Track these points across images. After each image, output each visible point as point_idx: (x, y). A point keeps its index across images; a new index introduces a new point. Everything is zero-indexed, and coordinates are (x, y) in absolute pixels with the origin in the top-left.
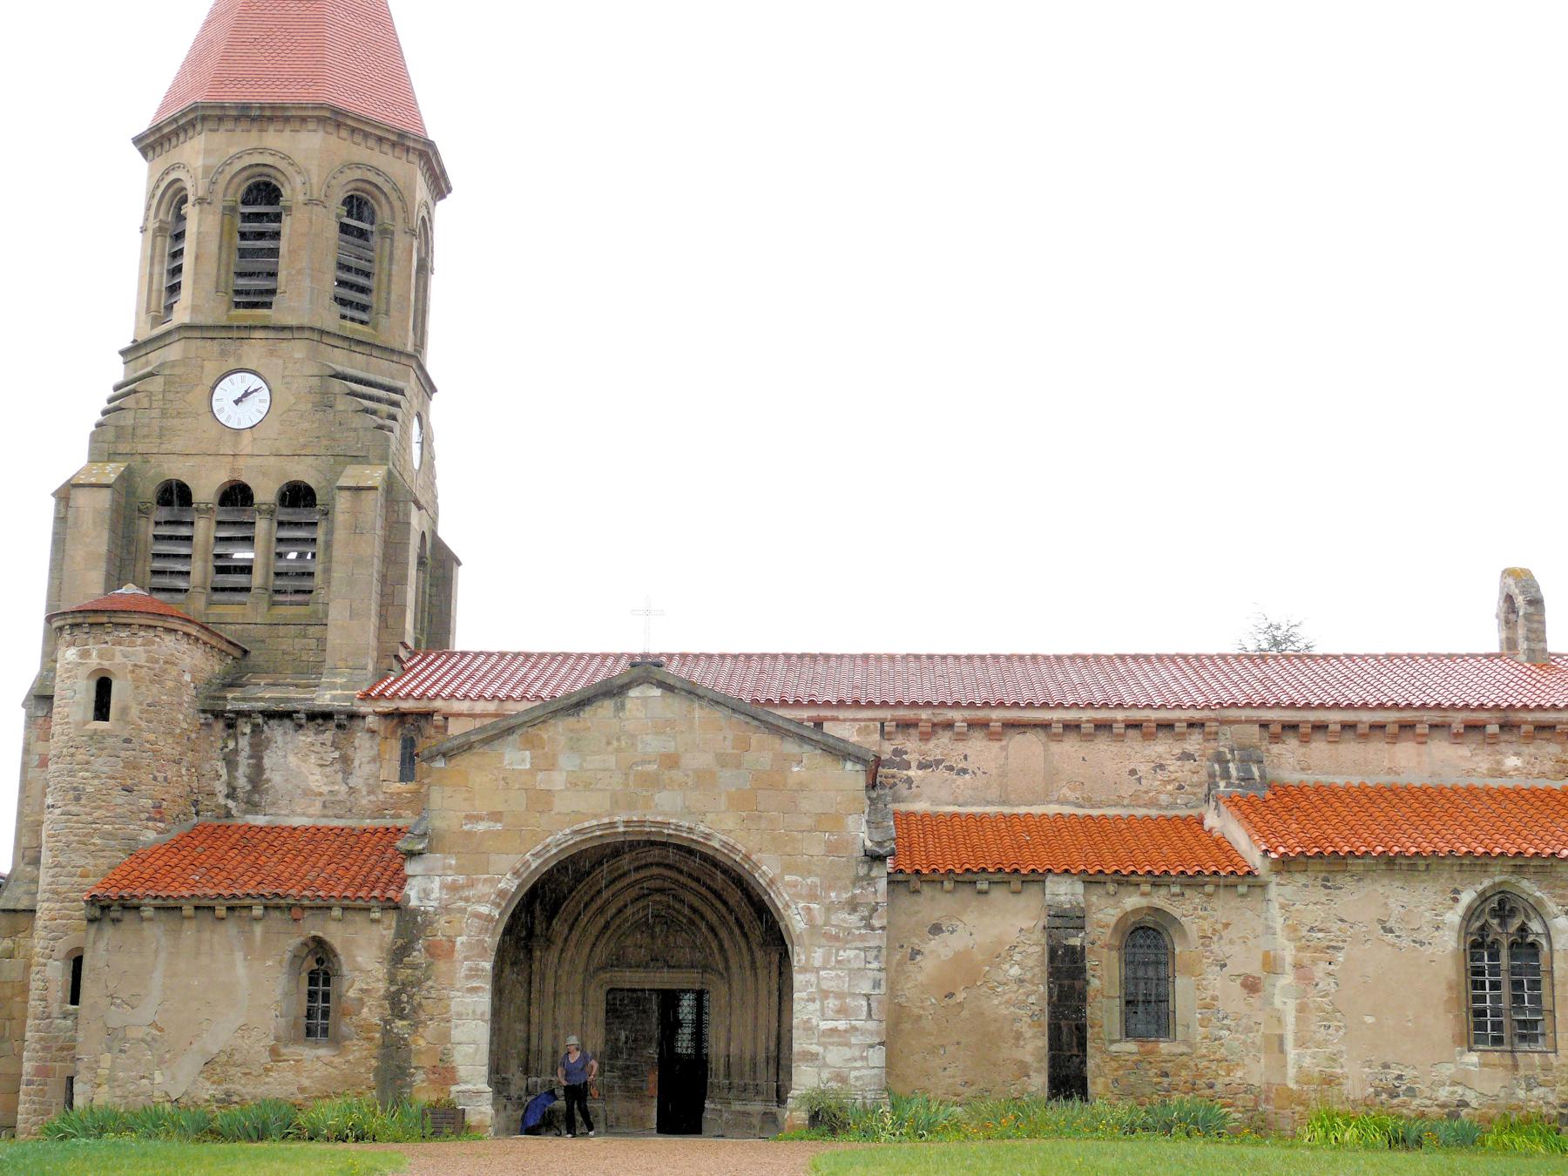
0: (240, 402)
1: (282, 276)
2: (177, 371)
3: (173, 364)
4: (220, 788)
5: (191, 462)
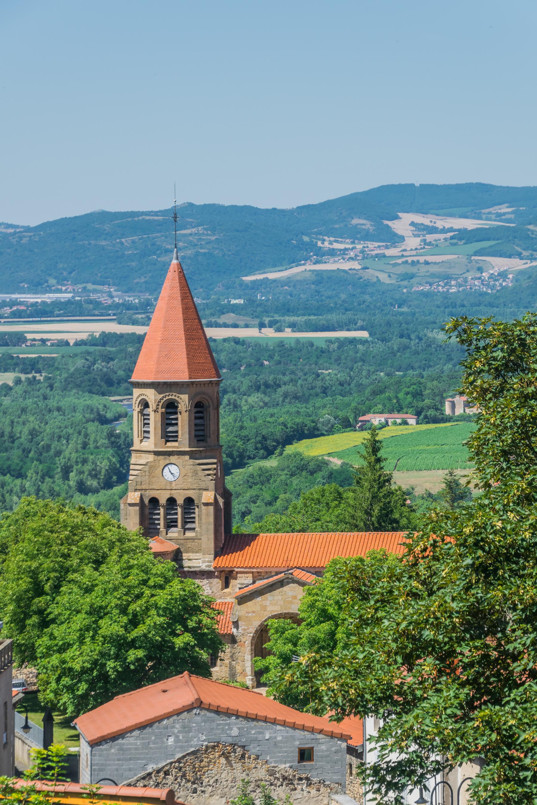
1: (180, 432)
2: (153, 464)
3: (151, 462)
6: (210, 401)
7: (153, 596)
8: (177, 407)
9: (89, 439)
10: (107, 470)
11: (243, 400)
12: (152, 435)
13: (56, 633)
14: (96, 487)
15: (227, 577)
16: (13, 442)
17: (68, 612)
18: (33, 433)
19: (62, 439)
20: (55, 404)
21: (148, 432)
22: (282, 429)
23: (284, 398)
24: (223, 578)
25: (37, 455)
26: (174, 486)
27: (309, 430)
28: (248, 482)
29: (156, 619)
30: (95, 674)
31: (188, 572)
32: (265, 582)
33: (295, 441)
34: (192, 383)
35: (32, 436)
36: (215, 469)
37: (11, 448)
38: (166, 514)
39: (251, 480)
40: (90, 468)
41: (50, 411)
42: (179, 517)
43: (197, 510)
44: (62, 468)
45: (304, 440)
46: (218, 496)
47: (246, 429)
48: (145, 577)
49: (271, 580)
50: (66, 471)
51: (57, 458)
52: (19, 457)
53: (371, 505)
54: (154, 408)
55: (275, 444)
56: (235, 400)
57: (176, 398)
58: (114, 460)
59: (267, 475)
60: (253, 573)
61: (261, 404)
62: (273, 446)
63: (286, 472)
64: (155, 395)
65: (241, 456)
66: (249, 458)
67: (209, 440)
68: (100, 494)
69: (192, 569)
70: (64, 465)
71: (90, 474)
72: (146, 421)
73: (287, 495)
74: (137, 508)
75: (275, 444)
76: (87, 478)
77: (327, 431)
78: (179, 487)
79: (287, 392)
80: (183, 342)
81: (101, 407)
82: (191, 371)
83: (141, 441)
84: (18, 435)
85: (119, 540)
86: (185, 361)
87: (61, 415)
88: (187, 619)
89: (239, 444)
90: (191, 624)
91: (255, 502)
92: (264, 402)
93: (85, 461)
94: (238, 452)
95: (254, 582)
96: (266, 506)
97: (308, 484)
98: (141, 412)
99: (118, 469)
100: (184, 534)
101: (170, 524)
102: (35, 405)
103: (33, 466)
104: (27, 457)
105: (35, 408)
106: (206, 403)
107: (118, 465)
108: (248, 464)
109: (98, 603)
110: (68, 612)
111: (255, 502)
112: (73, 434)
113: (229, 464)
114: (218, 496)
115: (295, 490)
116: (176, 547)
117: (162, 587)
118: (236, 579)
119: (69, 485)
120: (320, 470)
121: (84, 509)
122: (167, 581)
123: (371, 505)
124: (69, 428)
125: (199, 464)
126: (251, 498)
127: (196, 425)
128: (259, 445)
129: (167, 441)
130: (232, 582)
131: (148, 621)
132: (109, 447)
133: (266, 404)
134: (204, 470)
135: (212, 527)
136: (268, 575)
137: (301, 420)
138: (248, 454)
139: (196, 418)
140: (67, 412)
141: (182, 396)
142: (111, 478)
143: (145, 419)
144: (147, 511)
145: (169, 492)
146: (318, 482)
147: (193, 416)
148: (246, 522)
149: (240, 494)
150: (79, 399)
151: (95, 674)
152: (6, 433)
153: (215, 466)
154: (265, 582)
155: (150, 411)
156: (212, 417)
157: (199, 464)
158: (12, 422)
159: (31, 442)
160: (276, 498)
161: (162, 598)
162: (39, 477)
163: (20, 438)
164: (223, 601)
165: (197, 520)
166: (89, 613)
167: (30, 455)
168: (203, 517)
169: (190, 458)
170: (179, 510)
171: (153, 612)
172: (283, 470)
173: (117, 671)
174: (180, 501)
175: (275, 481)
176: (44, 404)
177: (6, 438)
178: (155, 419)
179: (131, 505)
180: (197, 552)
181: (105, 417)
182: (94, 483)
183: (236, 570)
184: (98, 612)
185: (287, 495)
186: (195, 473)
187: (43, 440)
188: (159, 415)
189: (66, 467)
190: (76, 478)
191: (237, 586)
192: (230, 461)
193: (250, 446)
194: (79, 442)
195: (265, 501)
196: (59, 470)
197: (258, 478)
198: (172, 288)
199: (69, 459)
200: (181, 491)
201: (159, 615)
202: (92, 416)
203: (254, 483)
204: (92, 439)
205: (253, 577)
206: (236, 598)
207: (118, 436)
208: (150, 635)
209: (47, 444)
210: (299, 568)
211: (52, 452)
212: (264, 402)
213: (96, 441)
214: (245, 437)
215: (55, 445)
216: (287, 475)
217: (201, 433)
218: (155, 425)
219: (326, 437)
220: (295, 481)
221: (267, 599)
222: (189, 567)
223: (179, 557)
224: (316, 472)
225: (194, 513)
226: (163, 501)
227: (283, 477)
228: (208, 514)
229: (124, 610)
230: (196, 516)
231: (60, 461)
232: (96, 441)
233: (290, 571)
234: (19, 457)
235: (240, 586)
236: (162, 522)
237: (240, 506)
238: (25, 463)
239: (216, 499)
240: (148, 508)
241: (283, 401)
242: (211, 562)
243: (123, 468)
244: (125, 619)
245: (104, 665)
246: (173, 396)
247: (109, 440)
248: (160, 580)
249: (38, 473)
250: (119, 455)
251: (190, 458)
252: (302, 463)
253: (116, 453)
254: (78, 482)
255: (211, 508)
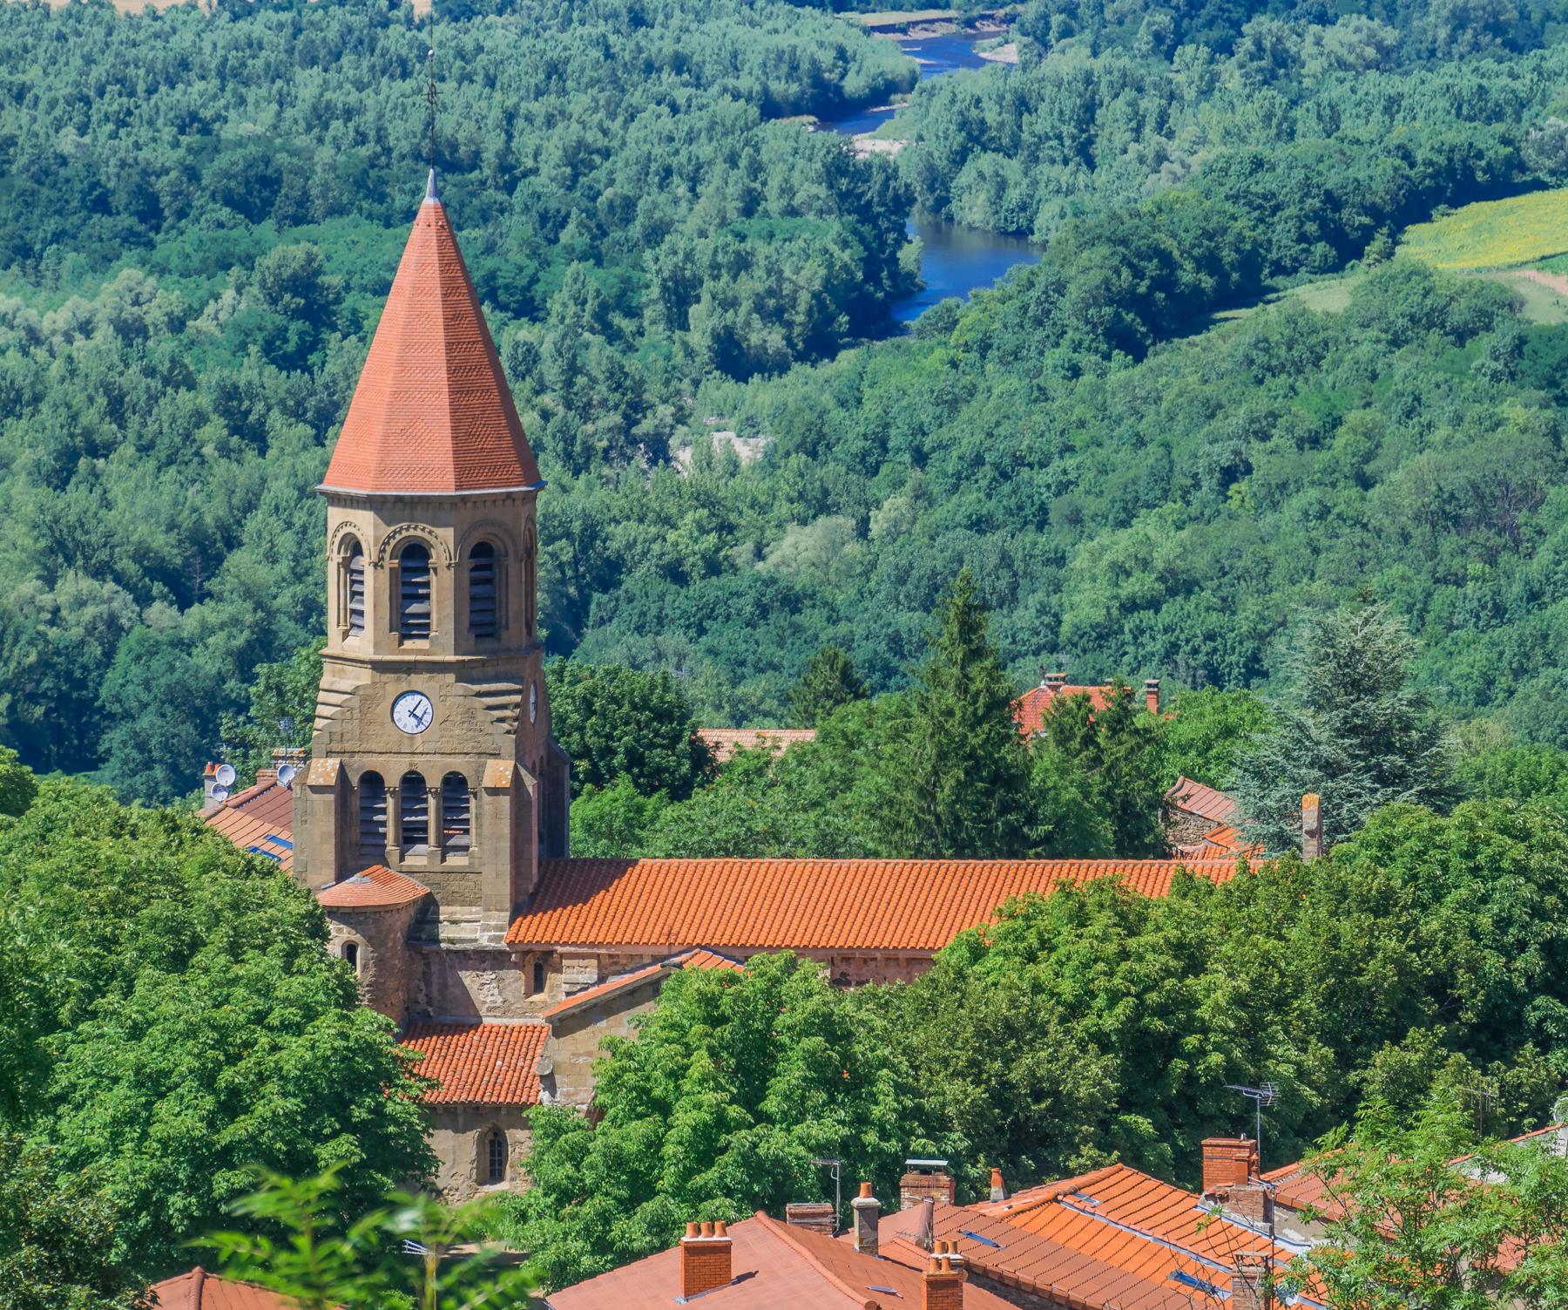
0: (413, 713)
1: (434, 616)
4: (421, 997)
5: (382, 758)
6: (508, 542)
7: (275, 1048)
8: (428, 556)
9: (764, 184)
10: (815, 295)
11: (1309, 39)
12: (368, 621)
13: (64, 1127)
14: (778, 352)
15: (539, 965)
16: (510, 188)
17: (92, 1081)
18: (579, 161)
19: (676, 179)
20: (668, 48)
21: (361, 613)
22: (1396, 169)
23: (1454, 30)
24: (531, 969)
25: (587, 238)
26: (419, 745)
27: (1488, 169)
28: (1252, 362)
29: (275, 1102)
30: (142, 1222)
31: (448, 951)
32: (627, 979)
33: (1442, 207)
34: (464, 499)
35: (574, 166)
36: (517, 706)
37: (502, 211)
38: (403, 811)
39: (1261, 358)
40: (760, 288)
41: (650, 68)
42: (431, 818)
43: (473, 804)
44: (665, 289)
45: (1474, 206)
46: (523, 772)
47: (1273, 168)
48: (261, 1005)
49: (640, 974)
50: (680, 295)
51: (648, 255)
52: (525, 242)
53: (936, 773)
54: (374, 558)
55: (1366, 220)
56: (1279, 40)
57: (426, 535)
58: (846, 256)
59: (1313, 340)
60: (598, 956)
61: (1370, 52)
62: (1362, 227)
63: (1373, 333)
64: (376, 526)
65: (1251, 262)
66: (1279, 269)
67: (504, 635)
68: (789, 378)
69: (458, 946)
70: (673, 277)
71: (759, 308)
72: (356, 587)
73: (1370, 415)
74: (331, 797)
75: (1366, 220)
76: (748, 324)
77: (1553, 173)
78: (431, 747)
79: (1465, 9)
80: (445, 400)
81: (826, 57)
82: (463, 474)
83: (346, 635)
84: (530, 163)
85: (234, 906)
86: (448, 445)
87: (685, 85)
88: (352, 1102)
89: (1239, 224)
90: (359, 1114)
91: (1264, 436)
92: (1380, 47)
93: (742, 264)
94: (1238, 251)
95: (602, 979)
96: (1300, 448)
97: (1441, 376)
98: (346, 564)
99: (859, 287)
100: (443, 860)
101: (411, 836)
102: (596, 53)
103: (568, 279)
104: (556, 241)
105: (596, 65)
106: (497, 545)
107: (860, 275)
108: (1275, 290)
109: (156, 1062)
110: (92, 1081)
111: (1264, 436)
112: (711, 163)
113: (1202, 291)
114: (523, 772)
115: (1399, 394)
116: (422, 890)
117: (298, 1030)
118: (559, 970)
119: (685, 345)
120: (1488, 328)
121: (173, 820)
122: (310, 1014)
123: (936, 773)
124: (703, 138)
125: (479, 695)
126: (1252, 421)
127: (473, 599)
128: (1311, 228)
129: (405, 636)
130: (552, 978)
131: (260, 1109)
132: (830, 212)
133: (1385, 51)
134: (490, 708)
135: (506, 846)
136: (636, 963)
137: (1463, 137)
138: (1274, 255)
139: (474, 582)
140: (708, 70)
141: (439, 531)
142: (831, 319)
143: (353, 582)
144: (356, 803)
145: (407, 759)
146: (1478, 370)
147: (466, 576)
148: (1234, 504)
149: (1220, 406)
150: (753, 24)
151: (142, 1222)
152: (489, 156)
153: (517, 698)
154: (627, 979)
155: (364, 562)
156: (512, 580)
157: (479, 695)
158: (510, 117)
159: (570, 188)
160: (1337, 422)
161: (295, 1053)
162: (587, 318)
163: (535, 171)
164: (529, 1022)
165: (473, 826)
166: (139, 1085)
167: (565, 236)
168: (486, 821)
169: (458, 680)
170: (432, 803)
171: (272, 1087)
172: (1365, 326)
173: (191, 1217)
174: (434, 781)
175: (1337, 363)
176: (631, 45)
177: (487, 172)
178: (375, 584)
179: (316, 789)
180: (471, 904)
181: (839, 90)
182: (774, 339)
183: (559, 949)
184: (154, 1084)
185: (1370, 415)
186: (470, 714)
187: (611, 182)
188: (385, 576)
189: (676, 283)
190: (710, 324)
191: (558, 993)
192: (1208, 282)
193: (1282, 233)
194: (730, 190)
195: (1299, 432)
196: (655, 292)
197: (1283, 351)
198: (422, 266)
199: (689, 257)
200: (437, 758)
201: (285, 1095)
202: (794, 88)
203: (1269, 369)
204: (775, 183)
205: (600, 967)
206: (549, 1020)
207: (861, 174)
208: (264, 1139)
209: (626, 198)
210: (706, 948)
211: (635, 230)
212: (1380, 47)
213: (788, 190)
214: (1264, 197)
215: (652, 202)
216: (1378, 341)
217: (487, 618)
218: (376, 597)
219: (1550, 194)
220: (1403, 363)
221: (620, 1024)
222: (451, 941)
223: (430, 916)
224: (1474, 333)
225: (467, 810)
226: (392, 780)
227: (1364, 351)
228: (496, 815)
229: (207, 1079)
230: (471, 816)
231: (657, 265)
232: (788, 190)
233: (677, 960)
234: (525, 242)
235: (566, 988)
236: (390, 831)
237: (1217, 448)
238: (545, 264)
239: (516, 776)
240: (358, 797)
241: (1452, 39)
242: (501, 929)
243: (878, 284)
244: (209, 1102)
245: (162, 1203)
246: (419, 531)
247: (831, 187)
248: (294, 1015)
249: (584, 302)
250: (862, 240)
251: (458, 680)
252: (1428, 302)
253: (855, 232)
254: (716, 337)
255: (505, 801)
